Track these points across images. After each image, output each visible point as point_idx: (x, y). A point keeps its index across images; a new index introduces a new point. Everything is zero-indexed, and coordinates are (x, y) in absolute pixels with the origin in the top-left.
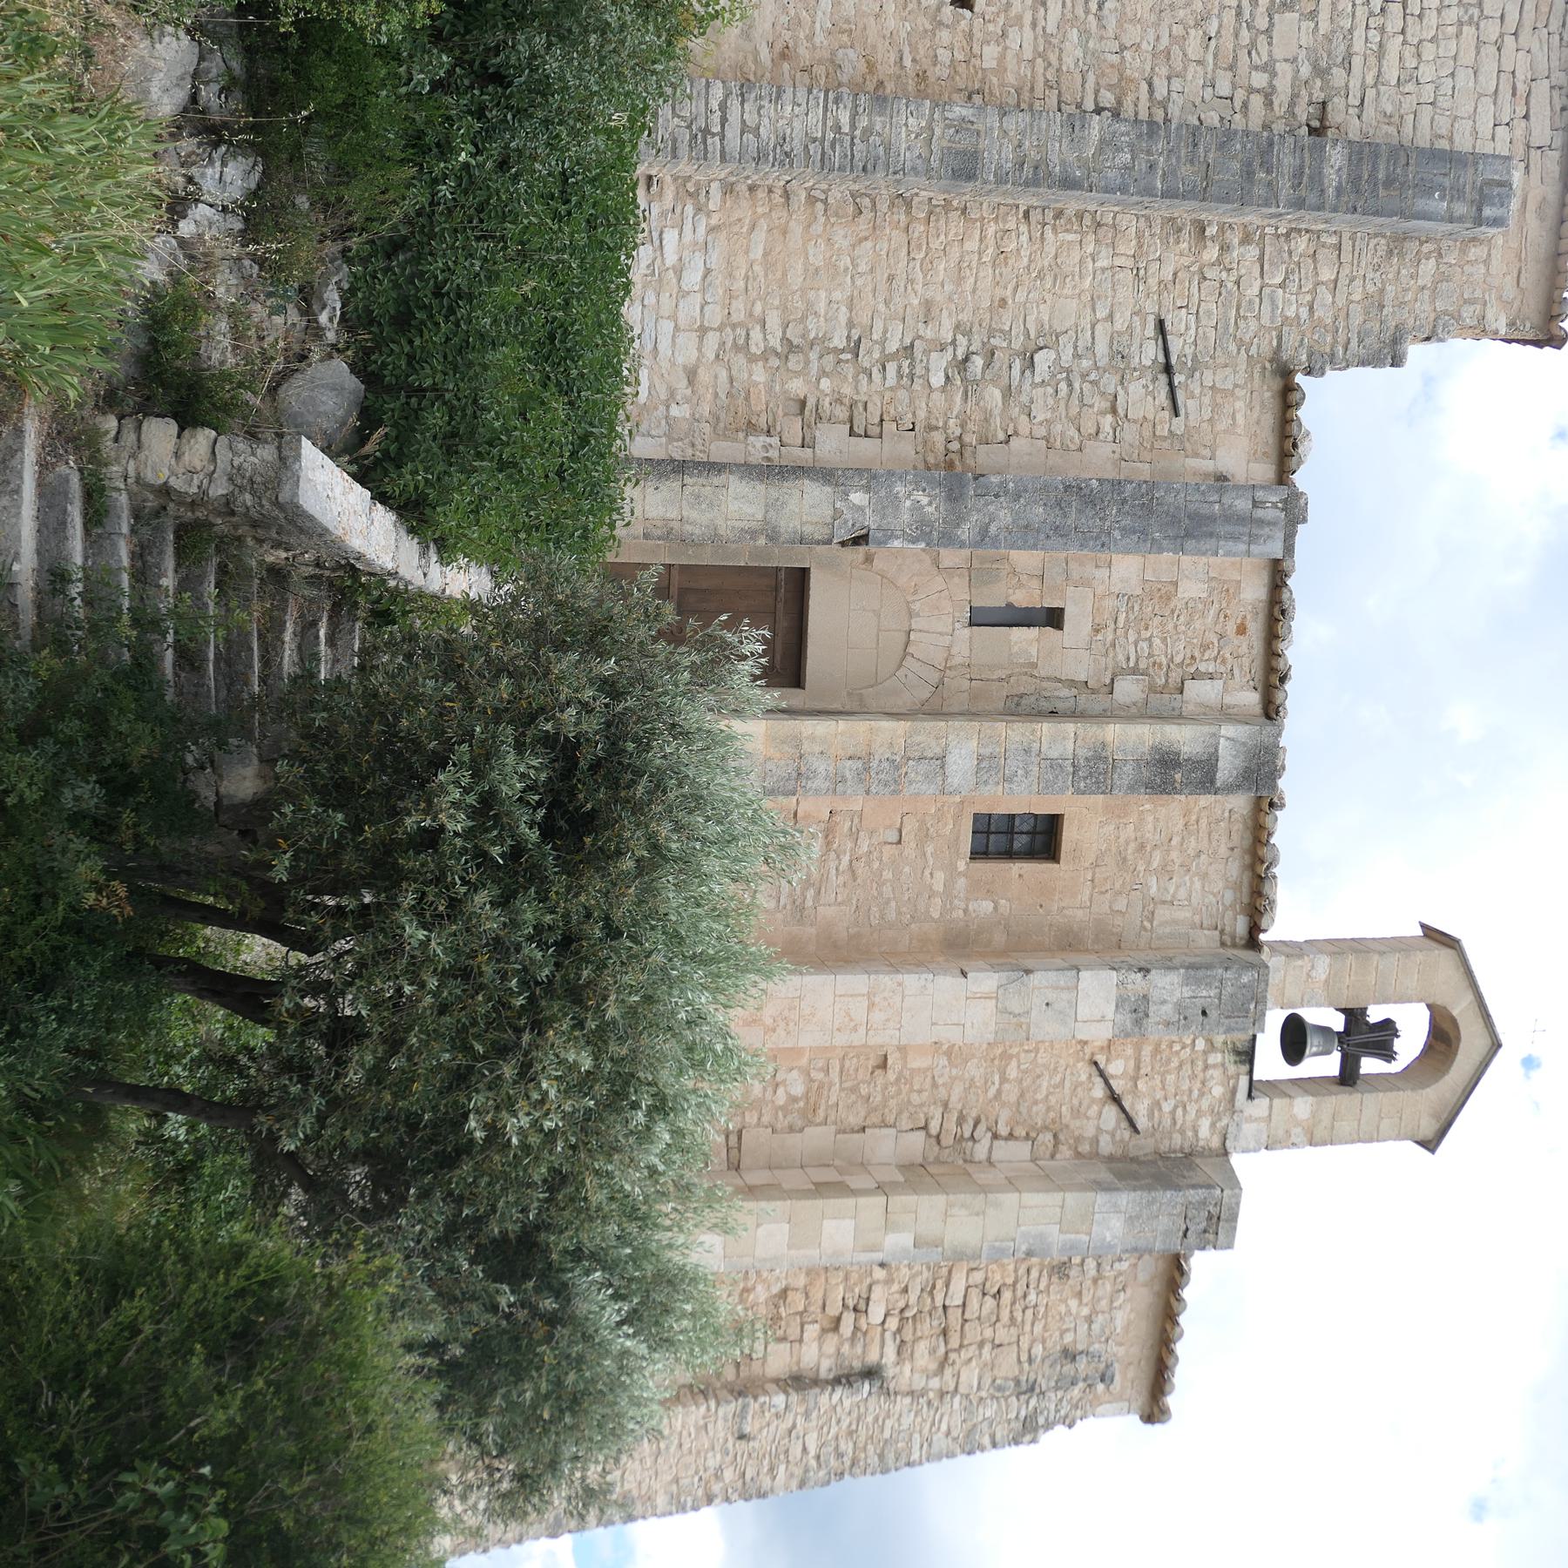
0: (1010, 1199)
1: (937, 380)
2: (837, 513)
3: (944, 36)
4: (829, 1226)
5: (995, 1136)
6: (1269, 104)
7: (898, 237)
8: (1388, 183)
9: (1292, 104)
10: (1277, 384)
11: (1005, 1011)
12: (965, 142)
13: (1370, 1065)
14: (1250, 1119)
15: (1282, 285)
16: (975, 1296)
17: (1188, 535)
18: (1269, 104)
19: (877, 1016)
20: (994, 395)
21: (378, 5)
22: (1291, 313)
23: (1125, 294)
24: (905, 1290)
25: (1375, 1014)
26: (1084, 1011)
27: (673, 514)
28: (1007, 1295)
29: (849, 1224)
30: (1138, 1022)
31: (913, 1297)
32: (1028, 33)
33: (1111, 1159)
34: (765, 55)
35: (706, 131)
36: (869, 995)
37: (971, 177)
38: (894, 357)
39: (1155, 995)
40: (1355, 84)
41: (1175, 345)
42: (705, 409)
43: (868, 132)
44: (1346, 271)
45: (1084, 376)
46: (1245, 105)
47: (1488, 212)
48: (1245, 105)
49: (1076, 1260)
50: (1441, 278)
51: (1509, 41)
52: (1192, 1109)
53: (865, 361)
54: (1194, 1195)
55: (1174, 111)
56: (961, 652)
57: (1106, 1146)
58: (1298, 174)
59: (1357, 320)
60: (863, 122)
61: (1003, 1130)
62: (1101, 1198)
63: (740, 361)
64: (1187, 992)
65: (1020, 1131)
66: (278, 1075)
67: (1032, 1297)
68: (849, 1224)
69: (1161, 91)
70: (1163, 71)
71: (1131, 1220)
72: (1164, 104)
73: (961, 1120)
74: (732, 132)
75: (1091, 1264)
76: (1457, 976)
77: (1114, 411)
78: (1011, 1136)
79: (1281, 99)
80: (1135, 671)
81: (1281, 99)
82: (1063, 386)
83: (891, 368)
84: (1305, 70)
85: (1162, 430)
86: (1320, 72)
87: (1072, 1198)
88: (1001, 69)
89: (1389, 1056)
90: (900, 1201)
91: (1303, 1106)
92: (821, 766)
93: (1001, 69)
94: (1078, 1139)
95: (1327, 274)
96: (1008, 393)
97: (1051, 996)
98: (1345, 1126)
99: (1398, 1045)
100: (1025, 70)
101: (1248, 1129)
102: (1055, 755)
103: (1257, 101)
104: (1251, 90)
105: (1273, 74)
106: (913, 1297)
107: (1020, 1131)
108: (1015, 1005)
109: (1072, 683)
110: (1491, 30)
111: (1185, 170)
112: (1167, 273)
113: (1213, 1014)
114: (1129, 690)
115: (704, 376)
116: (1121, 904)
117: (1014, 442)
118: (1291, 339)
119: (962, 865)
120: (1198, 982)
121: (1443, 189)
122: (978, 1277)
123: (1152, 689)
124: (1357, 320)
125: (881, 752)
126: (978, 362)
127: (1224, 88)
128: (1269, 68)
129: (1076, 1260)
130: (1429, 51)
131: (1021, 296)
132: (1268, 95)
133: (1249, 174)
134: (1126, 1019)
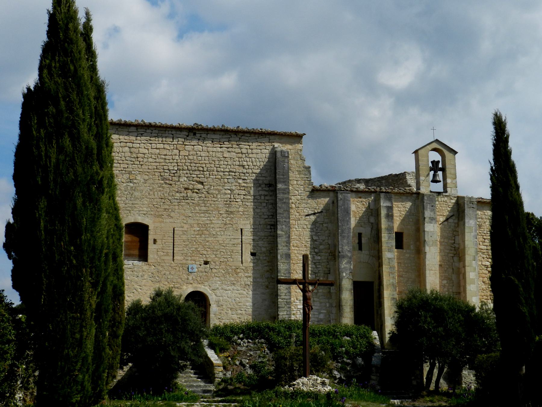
0: (466, 243)
1: (319, 258)
2: (347, 278)
3: (261, 258)
4: (471, 277)
5: (454, 243)
6: (266, 195)
7: (296, 266)
8: (283, 175)
9: (266, 191)
10: (315, 192)
11: (432, 245)
12: (284, 256)
13: (440, 166)
14: (451, 192)
15: (298, 191)
16: (484, 244)
17: (347, 213)
18: (266, 195)
19: (433, 269)
20: (321, 247)
21: (4, 344)
22: (303, 189)
23: (302, 222)
24: (483, 258)
25: (430, 165)
26: (432, 230)
27: (349, 307)
28: (485, 237)
29: (471, 273)
30: (434, 219)
31: (485, 256)
32: (259, 242)
33: (458, 220)
34: (268, 291)
35: (287, 302)
36: (430, 270)
37: (290, 255)
38: (316, 266)
39: (429, 216)
40: (261, 178)
41: (310, 212)
42: (327, 300)
43: (284, 274)
44: (294, 179)
45: (317, 230)
46: (267, 200)
47: (286, 155)
48: (267, 200)
49: (478, 223)
50: (294, 159)
51: (251, 147)
52: (450, 204)
53: (317, 271)
54: (466, 205)
55: (270, 214)
56: (367, 252)
57: (456, 221)
58: (283, 193)
59: (303, 176)
60: (282, 274)
61: (453, 241)
62: (466, 225)
63: (318, 294)
64: (429, 210)
65: (453, 238)
66: (363, 395)
67: (485, 232)
68: (471, 273)
69: (266, 217)
70: (263, 216)
71: (471, 219)
72: (268, 216)
73: (451, 250)
74: (286, 297)
75: (479, 220)
76: (423, 149)
77: (322, 224)
78: (454, 240)
79: (266, 193)
80: (369, 219)
81: (266, 193)
82: (319, 234)
83: (318, 266)
84: (260, 188)
85: (325, 214)
86: (260, 186)
87: (466, 231)
88: (266, 247)
89: (438, 162)
90: (467, 264)
91: (449, 181)
92: (391, 281)
93: (266, 247)
94: (455, 226)
95: (295, 182)
96: (321, 244)
97: (429, 236)
98: (453, 171)
99: (436, 160)
100: (265, 243)
101: (453, 192)
102: (387, 238)
103: (267, 198)
104: (265, 199)
105: (261, 195)
106: (485, 256)
107: (453, 238)
108: (431, 243)
109: (371, 231)
110: (250, 151)
111: (285, 215)
112: (298, 214)
113: (433, 204)
114: (372, 220)
115: (322, 301)
116: (411, 220)
117: (330, 243)
118: (307, 189)
119: (405, 251)
120: (427, 207)
121: (283, 165)
122: (481, 243)
123: (372, 215)
124: (303, 176)
125: (388, 270)
126: (316, 250)
127: (265, 204)
128: (260, 195)
129: (478, 223)
130: (255, 164)
131: (304, 242)
132: (265, 196)
133: (285, 203)
134: (434, 221)
